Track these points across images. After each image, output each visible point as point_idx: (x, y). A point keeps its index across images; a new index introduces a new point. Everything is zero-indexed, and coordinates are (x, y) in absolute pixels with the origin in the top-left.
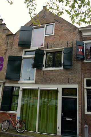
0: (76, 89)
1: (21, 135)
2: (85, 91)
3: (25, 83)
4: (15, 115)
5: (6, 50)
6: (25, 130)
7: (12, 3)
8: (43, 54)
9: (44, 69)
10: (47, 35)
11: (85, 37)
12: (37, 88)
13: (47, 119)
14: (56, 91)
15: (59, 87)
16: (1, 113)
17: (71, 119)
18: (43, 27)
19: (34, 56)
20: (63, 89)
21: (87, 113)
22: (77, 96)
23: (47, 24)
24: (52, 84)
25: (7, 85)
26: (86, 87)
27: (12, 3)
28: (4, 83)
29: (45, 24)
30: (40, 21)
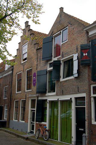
0: (85, 97)
1: (46, 142)
2: (92, 99)
3: (50, 96)
4: (45, 125)
5: (37, 65)
6: (49, 138)
7: (44, 12)
8: (60, 64)
9: (62, 80)
10: (64, 41)
11: (92, 36)
12: (57, 99)
13: (67, 130)
14: (70, 101)
15: (73, 97)
16: (90, 142)
17: (80, 129)
18: (60, 34)
19: (52, 69)
20: (76, 99)
21: (94, 123)
22: (85, 105)
23: (63, 30)
24: (67, 94)
25: (40, 98)
26: (92, 95)
27: (44, 12)
28: (38, 97)
29: (61, 30)
30: (4, 58)
